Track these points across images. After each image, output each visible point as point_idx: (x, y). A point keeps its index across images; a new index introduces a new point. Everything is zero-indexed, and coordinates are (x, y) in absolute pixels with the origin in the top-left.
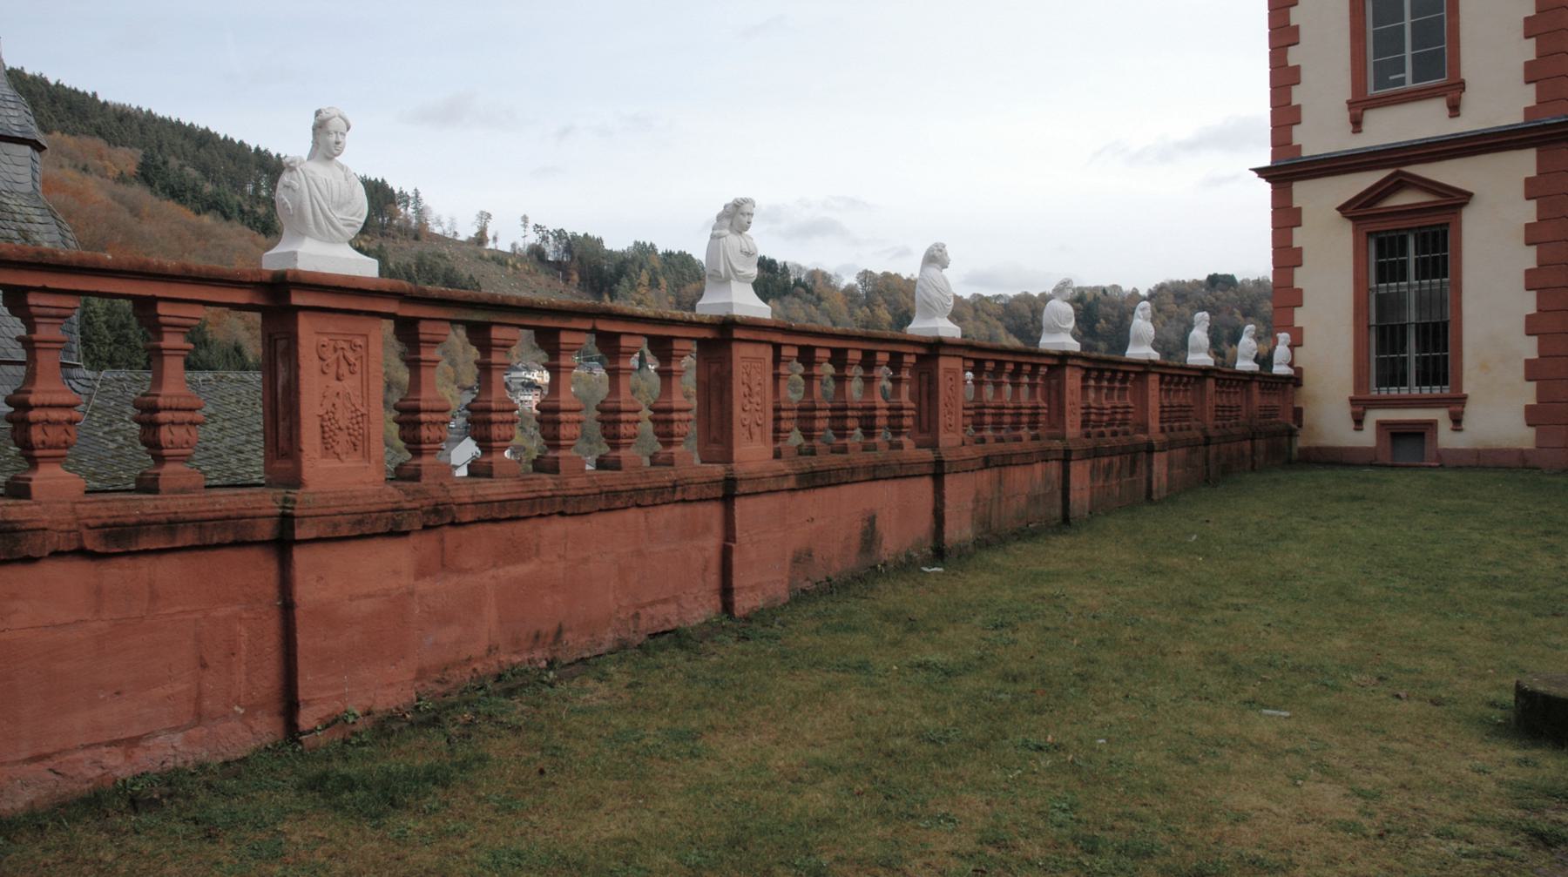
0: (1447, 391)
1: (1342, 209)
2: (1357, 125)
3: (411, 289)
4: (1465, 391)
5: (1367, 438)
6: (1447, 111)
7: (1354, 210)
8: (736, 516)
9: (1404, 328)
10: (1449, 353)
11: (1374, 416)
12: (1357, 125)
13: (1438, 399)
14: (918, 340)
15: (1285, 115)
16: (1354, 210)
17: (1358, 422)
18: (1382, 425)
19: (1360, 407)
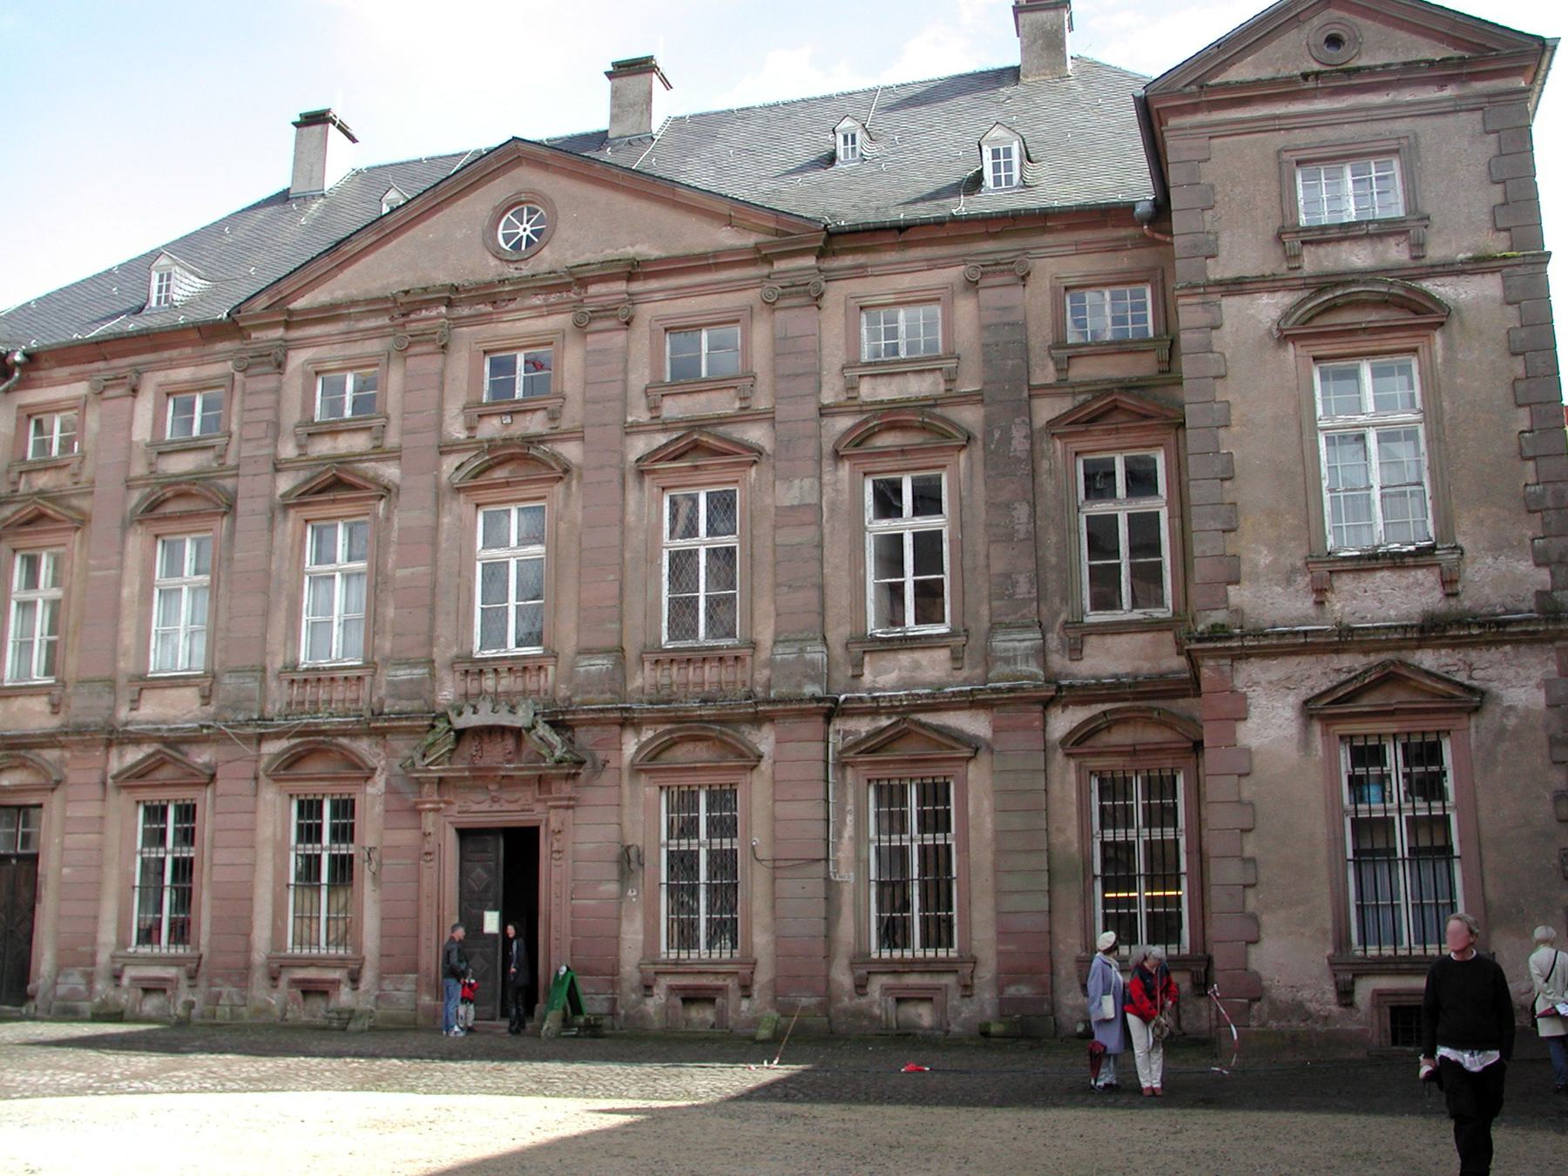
17: (1345, 995)
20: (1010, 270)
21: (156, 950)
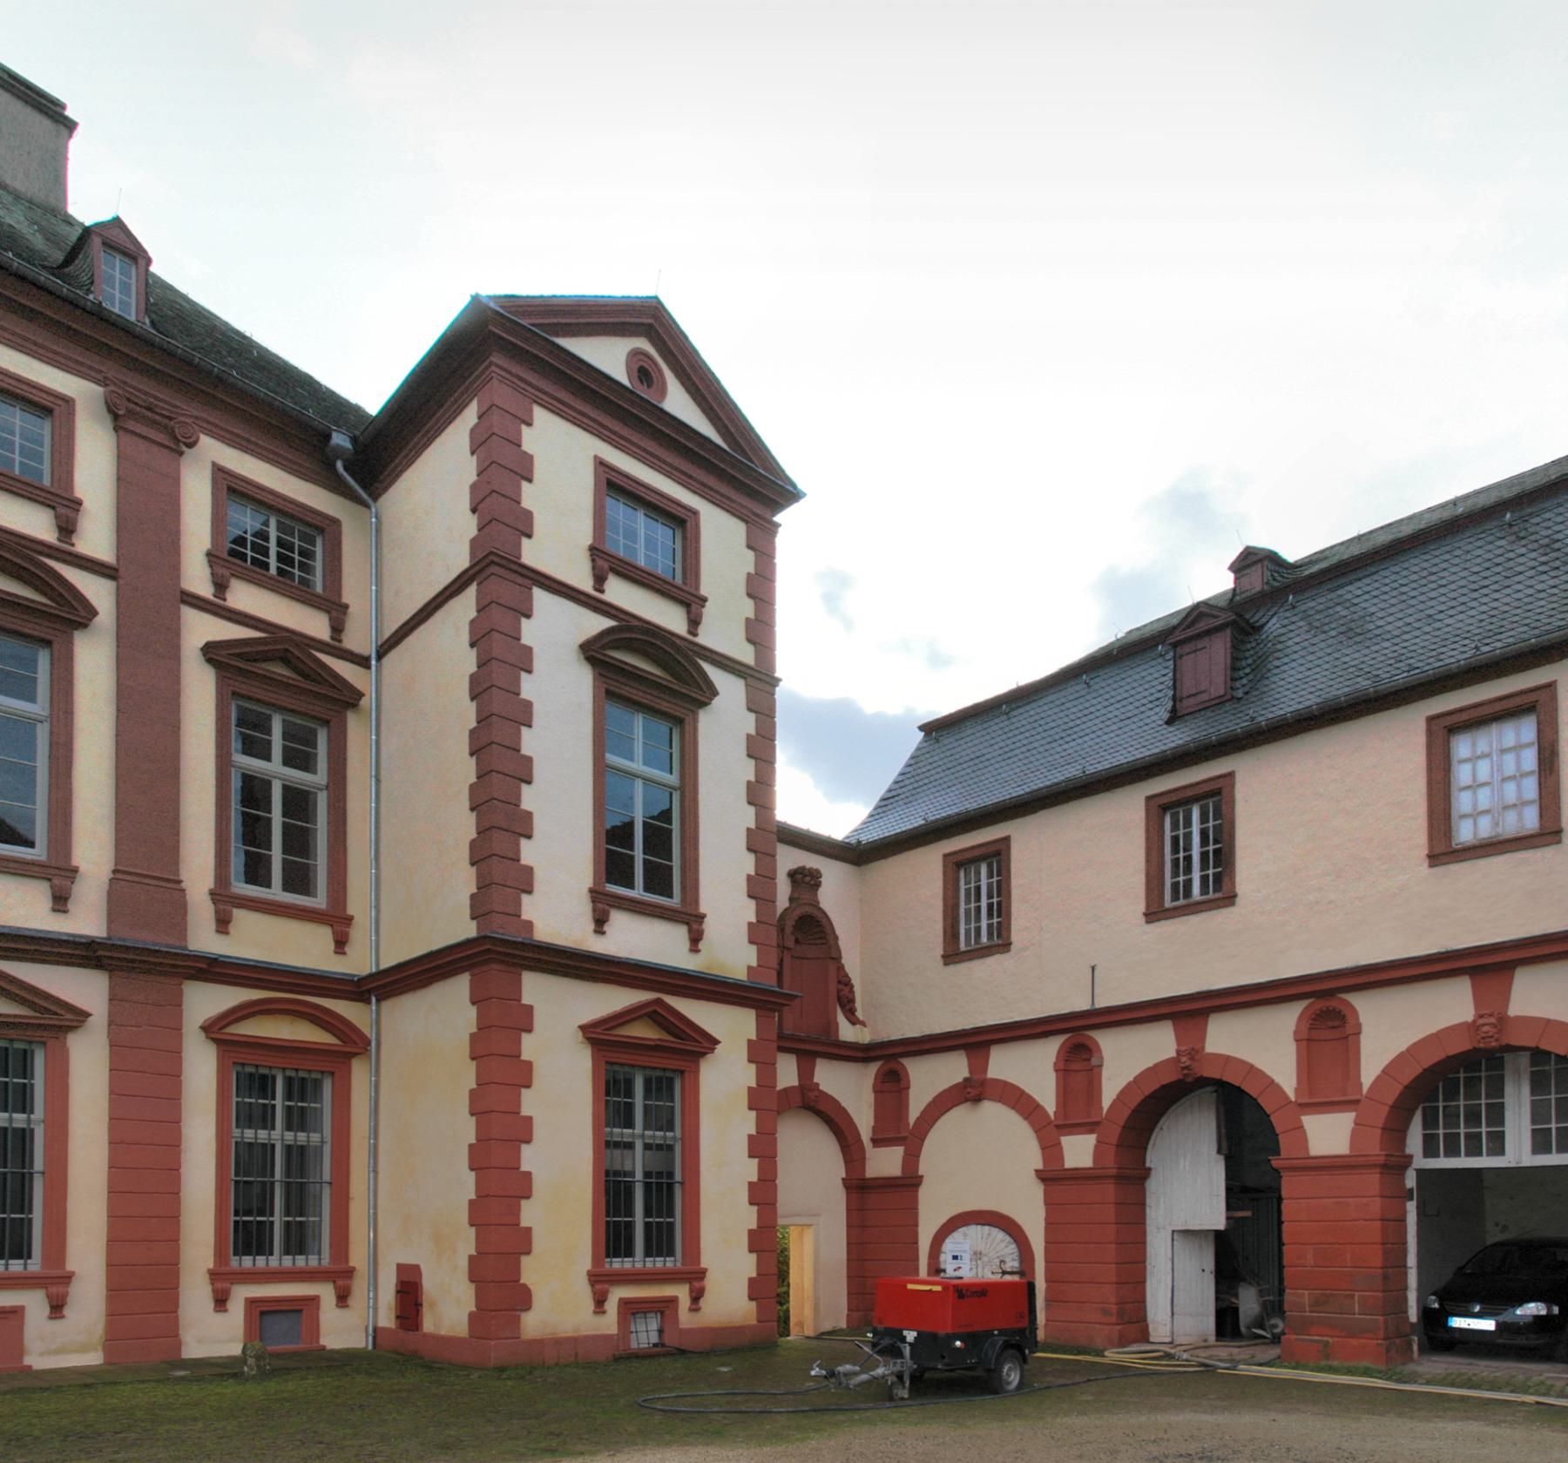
0: (35, 1265)
1: (584, 1028)
2: (600, 923)
3: (1009, 1383)
4: (352, 1264)
5: (609, 1323)
7: (599, 1035)
8: (975, 806)
9: (272, 1184)
10: (233, 1218)
11: (241, 1294)
12: (600, 923)
13: (303, 1272)
14: (1541, 480)
15: (1002, 889)
16: (599, 1035)
17: (600, 1303)
18: (251, 1303)
19: (600, 1282)
21: (669, 1265)
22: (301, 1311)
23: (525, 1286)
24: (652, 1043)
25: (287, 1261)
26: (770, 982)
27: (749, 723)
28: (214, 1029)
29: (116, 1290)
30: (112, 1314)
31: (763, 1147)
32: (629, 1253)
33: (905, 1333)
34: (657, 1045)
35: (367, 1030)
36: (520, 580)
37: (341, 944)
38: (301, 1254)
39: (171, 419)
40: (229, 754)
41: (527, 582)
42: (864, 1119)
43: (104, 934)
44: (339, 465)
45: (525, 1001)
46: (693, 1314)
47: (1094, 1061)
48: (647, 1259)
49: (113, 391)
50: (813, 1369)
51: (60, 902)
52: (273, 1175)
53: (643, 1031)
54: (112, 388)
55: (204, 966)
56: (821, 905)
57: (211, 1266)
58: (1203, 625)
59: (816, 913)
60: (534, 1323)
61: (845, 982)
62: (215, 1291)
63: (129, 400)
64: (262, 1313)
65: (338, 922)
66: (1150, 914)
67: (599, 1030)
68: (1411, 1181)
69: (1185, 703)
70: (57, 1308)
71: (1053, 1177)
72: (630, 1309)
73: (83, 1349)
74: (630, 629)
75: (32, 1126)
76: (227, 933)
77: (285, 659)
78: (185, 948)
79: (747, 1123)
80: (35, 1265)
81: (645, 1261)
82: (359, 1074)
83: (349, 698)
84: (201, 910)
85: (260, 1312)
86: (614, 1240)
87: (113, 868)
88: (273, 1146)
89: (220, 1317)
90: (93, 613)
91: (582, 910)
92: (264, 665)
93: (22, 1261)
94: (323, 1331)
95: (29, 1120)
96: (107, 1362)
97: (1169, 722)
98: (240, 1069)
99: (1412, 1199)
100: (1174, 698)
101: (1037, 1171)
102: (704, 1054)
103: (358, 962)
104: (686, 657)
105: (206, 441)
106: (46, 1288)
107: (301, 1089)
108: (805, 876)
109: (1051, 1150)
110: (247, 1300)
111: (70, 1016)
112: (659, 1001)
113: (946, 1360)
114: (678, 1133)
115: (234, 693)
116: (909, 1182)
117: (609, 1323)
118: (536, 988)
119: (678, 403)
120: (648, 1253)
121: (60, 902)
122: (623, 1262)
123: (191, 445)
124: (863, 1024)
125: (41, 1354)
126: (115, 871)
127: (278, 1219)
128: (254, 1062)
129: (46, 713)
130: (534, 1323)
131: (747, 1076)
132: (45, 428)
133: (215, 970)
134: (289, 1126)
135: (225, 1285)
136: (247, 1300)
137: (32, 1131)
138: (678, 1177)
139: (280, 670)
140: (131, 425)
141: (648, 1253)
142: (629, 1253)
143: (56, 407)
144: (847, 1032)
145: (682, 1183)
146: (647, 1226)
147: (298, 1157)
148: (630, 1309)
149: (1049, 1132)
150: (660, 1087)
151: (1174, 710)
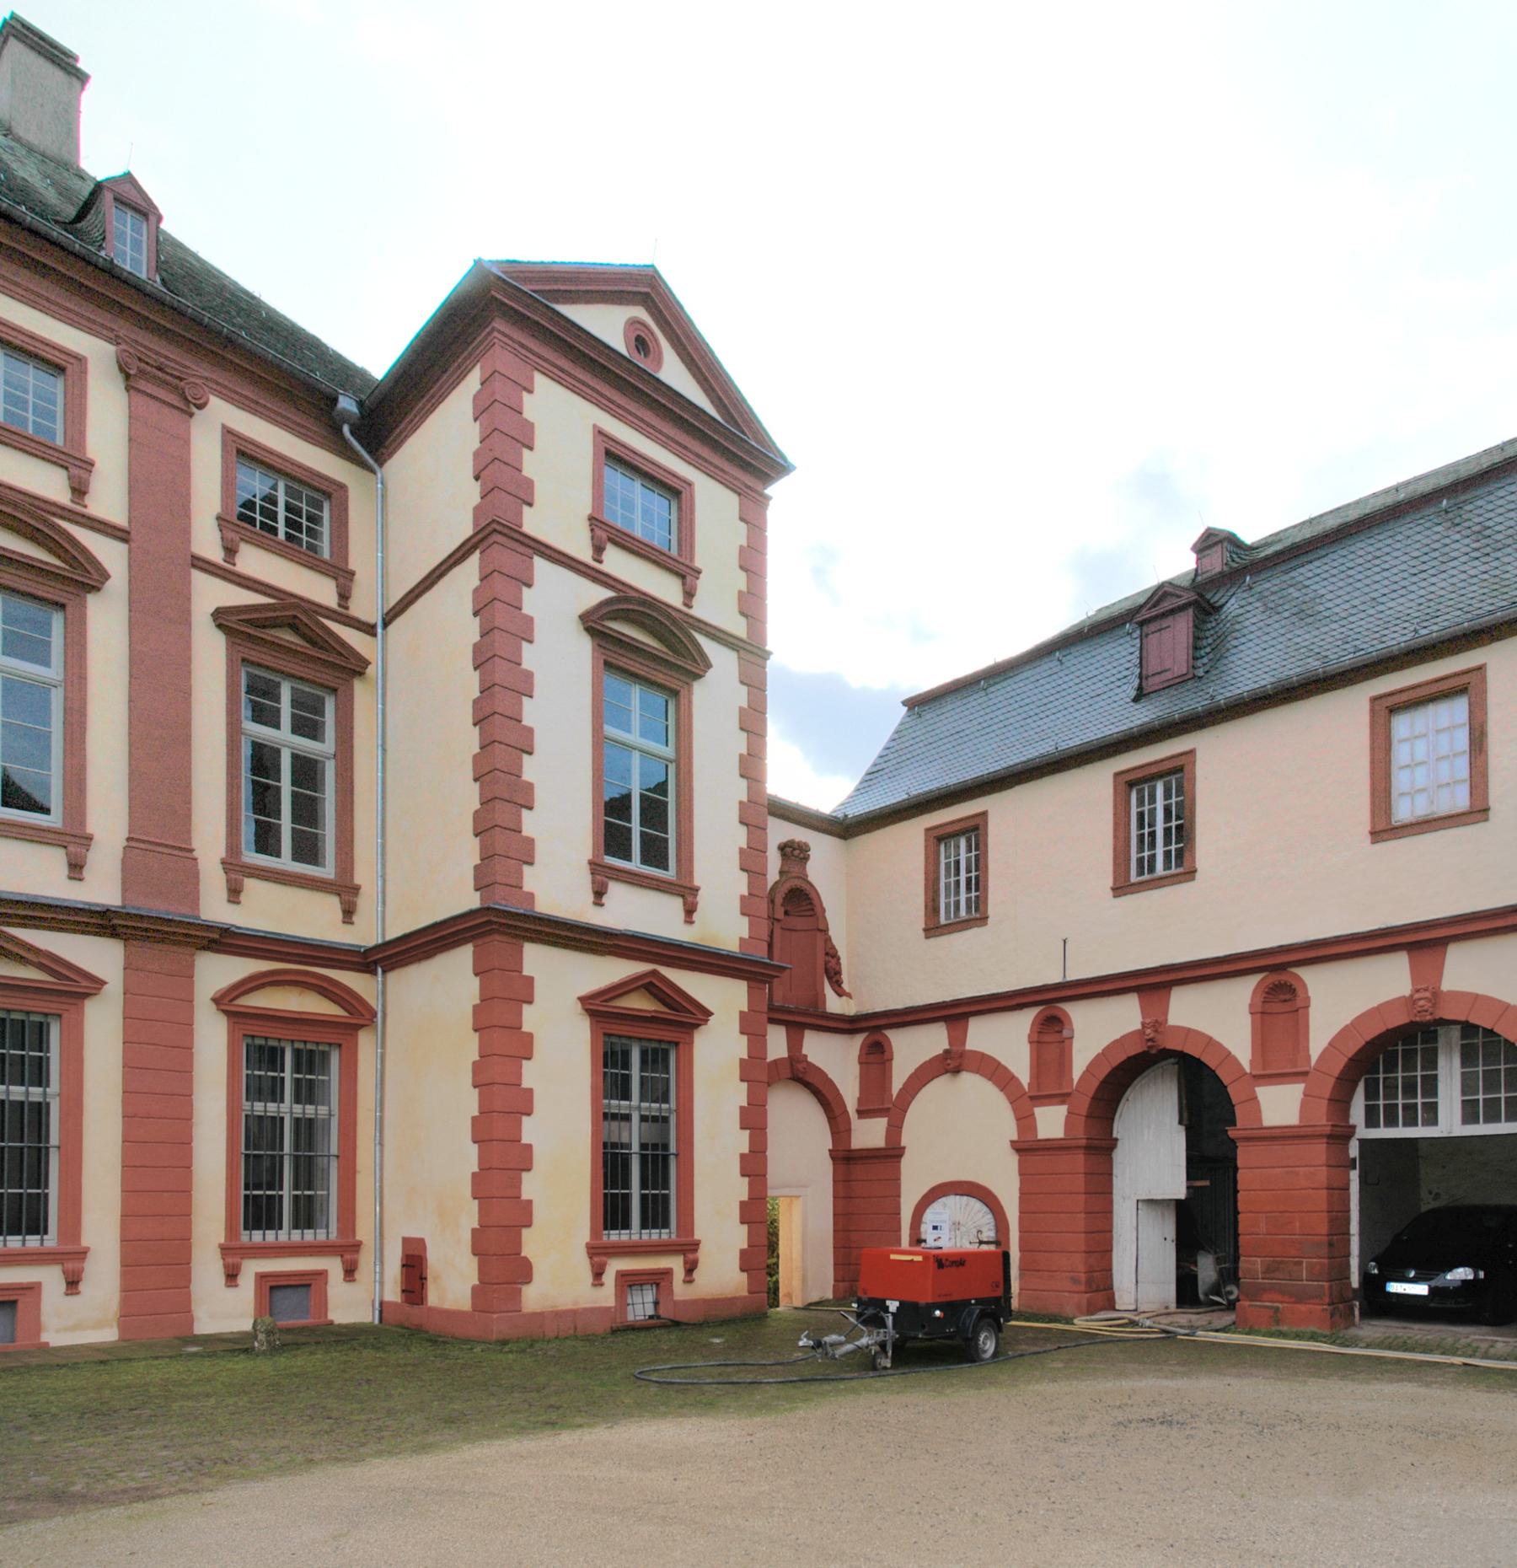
1: (583, 1000)
2: (599, 894)
4: (697, 1237)
5: (606, 1295)
6: (340, 915)
11: (251, 1269)
12: (599, 894)
17: (598, 1275)
18: (261, 1277)
19: (598, 1253)
20: (176, 388)
21: (665, 1237)
22: (309, 1285)
23: (525, 1258)
24: (649, 1015)
25: (296, 1235)
26: (760, 954)
27: (741, 696)
28: (225, 1001)
29: (129, 1265)
30: (127, 1289)
31: (754, 1119)
32: (626, 1225)
33: (888, 1303)
34: (653, 1017)
35: (374, 1002)
36: (522, 549)
37: (348, 913)
38: (309, 1228)
39: (181, 379)
40: (239, 721)
41: (529, 551)
42: (849, 1090)
43: (119, 903)
44: (346, 429)
45: (526, 972)
46: (687, 1285)
47: (1066, 1033)
48: (643, 1231)
49: (125, 351)
50: (801, 1340)
51: (76, 868)
52: (282, 1149)
53: (639, 1003)
54: (123, 347)
55: (216, 936)
56: (809, 879)
57: (222, 1240)
58: (1167, 605)
59: (804, 886)
60: (536, 1296)
61: (832, 954)
62: (226, 1266)
63: (140, 359)
64: (272, 1288)
65: (346, 892)
66: (1117, 888)
67: (597, 1002)
68: (1354, 1151)
69: (1151, 681)
70: (73, 1284)
71: (1027, 1148)
72: (628, 1281)
73: (99, 1325)
74: (627, 599)
75: (48, 1100)
76: (239, 903)
77: (294, 626)
78: (198, 918)
79: (739, 1095)
80: (51, 1241)
81: (641, 1234)
82: (366, 1043)
83: (355, 666)
84: (213, 881)
85: (272, 1288)
86: (612, 1213)
87: (127, 836)
88: (282, 1119)
89: (232, 1292)
90: (105, 576)
91: (583, 881)
92: (273, 632)
93: (39, 1237)
94: (330, 1306)
95: (45, 1094)
96: (122, 1339)
97: (1136, 700)
98: (249, 1041)
99: (1355, 1168)
100: (1140, 676)
101: (1012, 1142)
102: (697, 1026)
103: (364, 934)
104: (681, 629)
105: (215, 402)
106: (63, 1264)
107: (309, 1061)
108: (794, 849)
109: (1025, 1121)
110: (257, 1274)
111: (85, 983)
112: (654, 973)
113: (926, 1329)
114: (673, 1104)
115: (244, 660)
116: (892, 1153)
117: (606, 1295)
118: (537, 959)
119: (673, 373)
120: (644, 1225)
121: (76, 868)
122: (620, 1234)
123: (200, 407)
124: (849, 996)
125: (58, 1331)
126: (128, 839)
127: (287, 1193)
128: (263, 1034)
129: (61, 677)
130: (536, 1296)
131: (739, 1047)
132: (58, 386)
133: (226, 940)
134: (297, 1099)
135: (236, 1260)
136: (257, 1274)
137: (48, 1104)
138: (673, 1149)
139: (287, 637)
140: (142, 385)
141: (644, 1225)
142: (626, 1225)
143: (68, 365)
144: (834, 1004)
145: (677, 1155)
146: (644, 1198)
147: (307, 1130)
148: (628, 1281)
149: (1024, 1103)
150: (655, 1058)
151: (1140, 688)
